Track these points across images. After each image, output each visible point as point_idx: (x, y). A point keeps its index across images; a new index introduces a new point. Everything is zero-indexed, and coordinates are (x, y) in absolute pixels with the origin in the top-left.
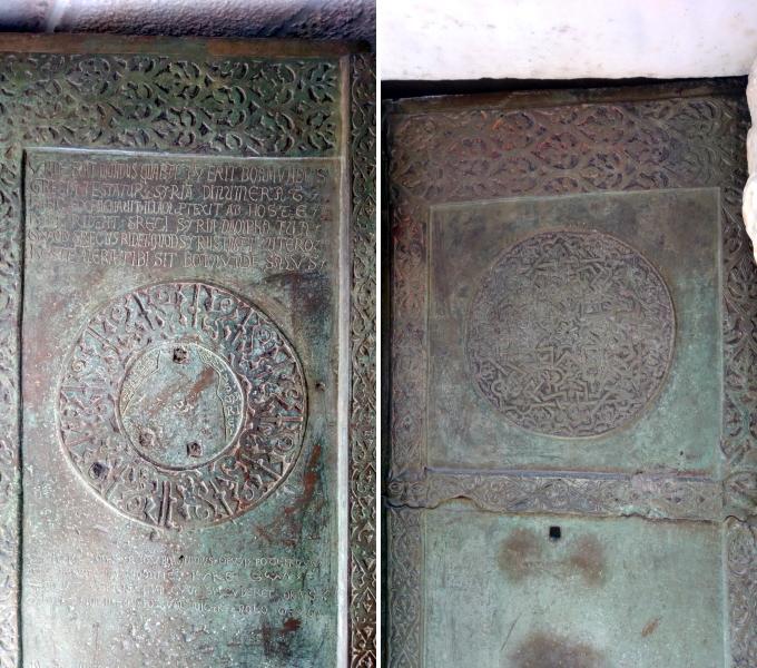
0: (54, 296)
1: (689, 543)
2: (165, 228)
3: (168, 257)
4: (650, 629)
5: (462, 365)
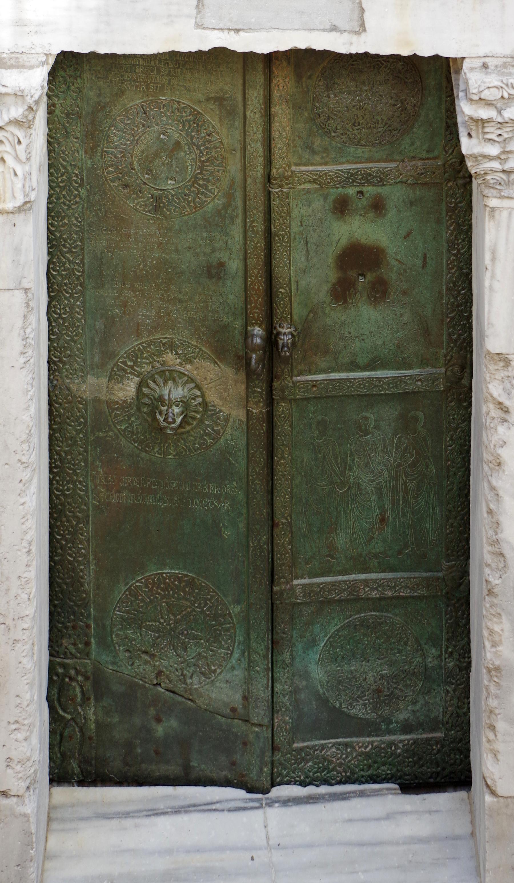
0: (99, 103)
3: (157, 87)
4: (408, 234)
5: (309, 114)
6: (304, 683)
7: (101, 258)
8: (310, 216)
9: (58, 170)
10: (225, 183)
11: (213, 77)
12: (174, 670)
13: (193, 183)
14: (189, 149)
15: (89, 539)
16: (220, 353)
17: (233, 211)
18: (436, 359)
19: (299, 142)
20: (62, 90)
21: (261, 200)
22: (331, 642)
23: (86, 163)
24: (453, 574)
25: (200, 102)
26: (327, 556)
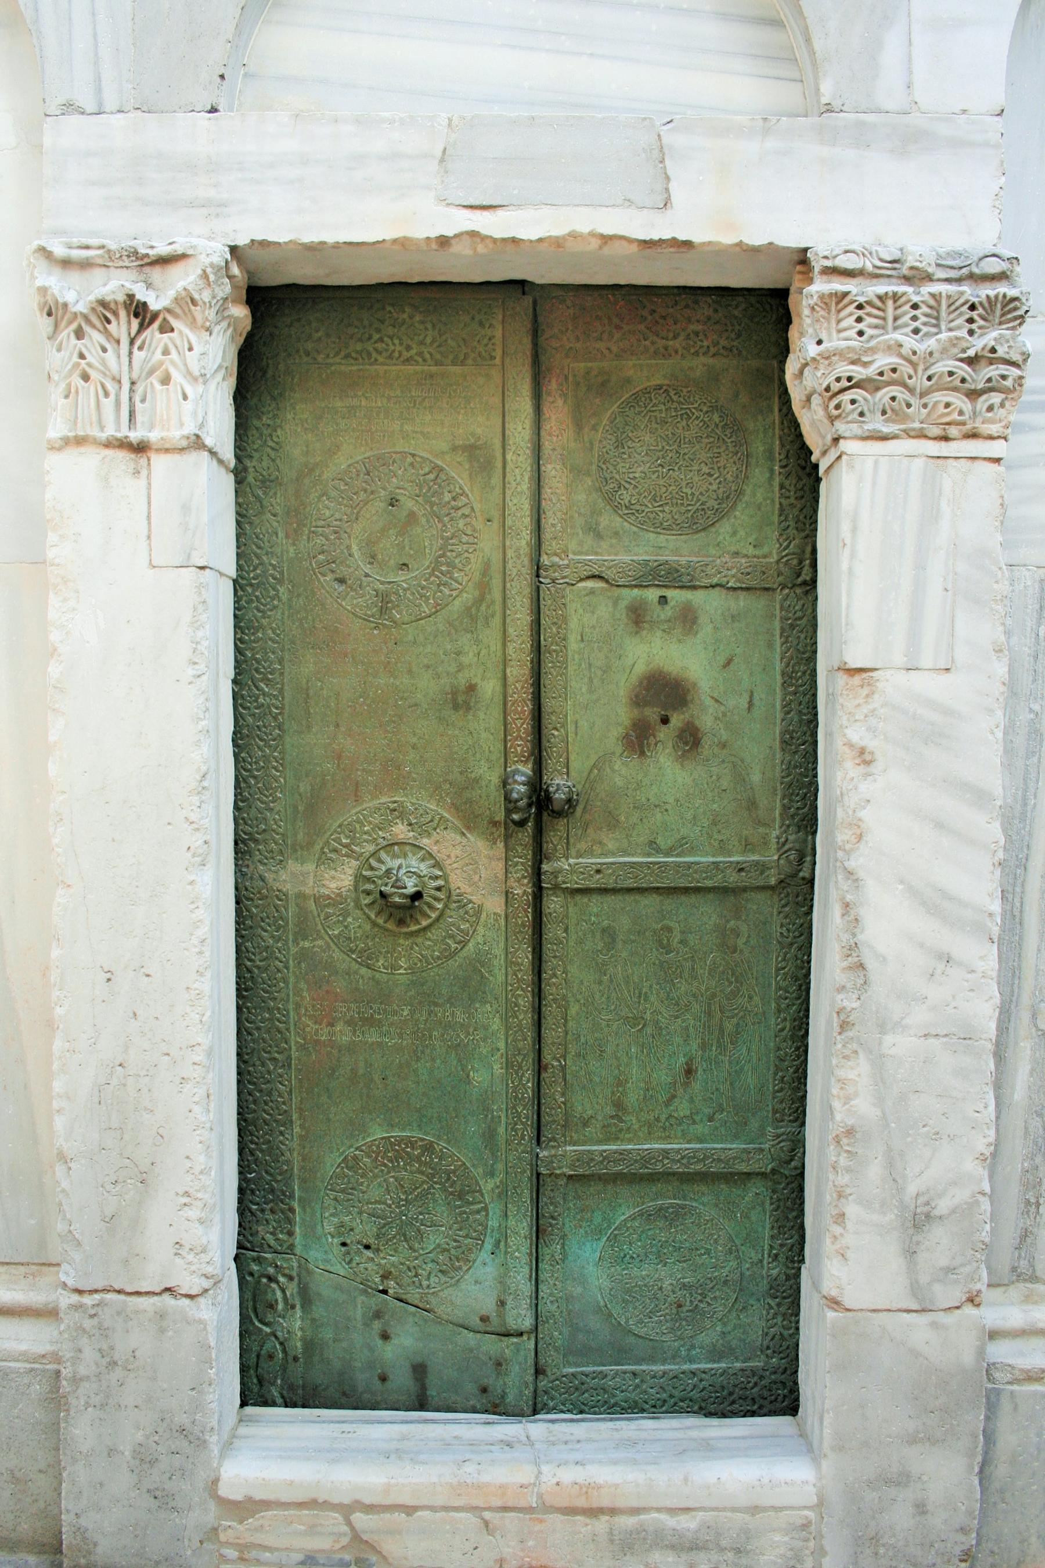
1: (756, 604)
2: (382, 415)
4: (729, 662)
6: (579, 1290)
7: (307, 689)
8: (593, 627)
9: (248, 561)
10: (475, 565)
11: (460, 417)
12: (405, 1268)
13: (433, 570)
14: (428, 521)
15: (291, 1090)
16: (470, 819)
17: (488, 607)
18: (765, 844)
19: (579, 521)
20: (255, 447)
21: (526, 579)
22: (616, 1235)
23: (287, 552)
24: (782, 1144)
25: (443, 453)
26: (612, 1117)
